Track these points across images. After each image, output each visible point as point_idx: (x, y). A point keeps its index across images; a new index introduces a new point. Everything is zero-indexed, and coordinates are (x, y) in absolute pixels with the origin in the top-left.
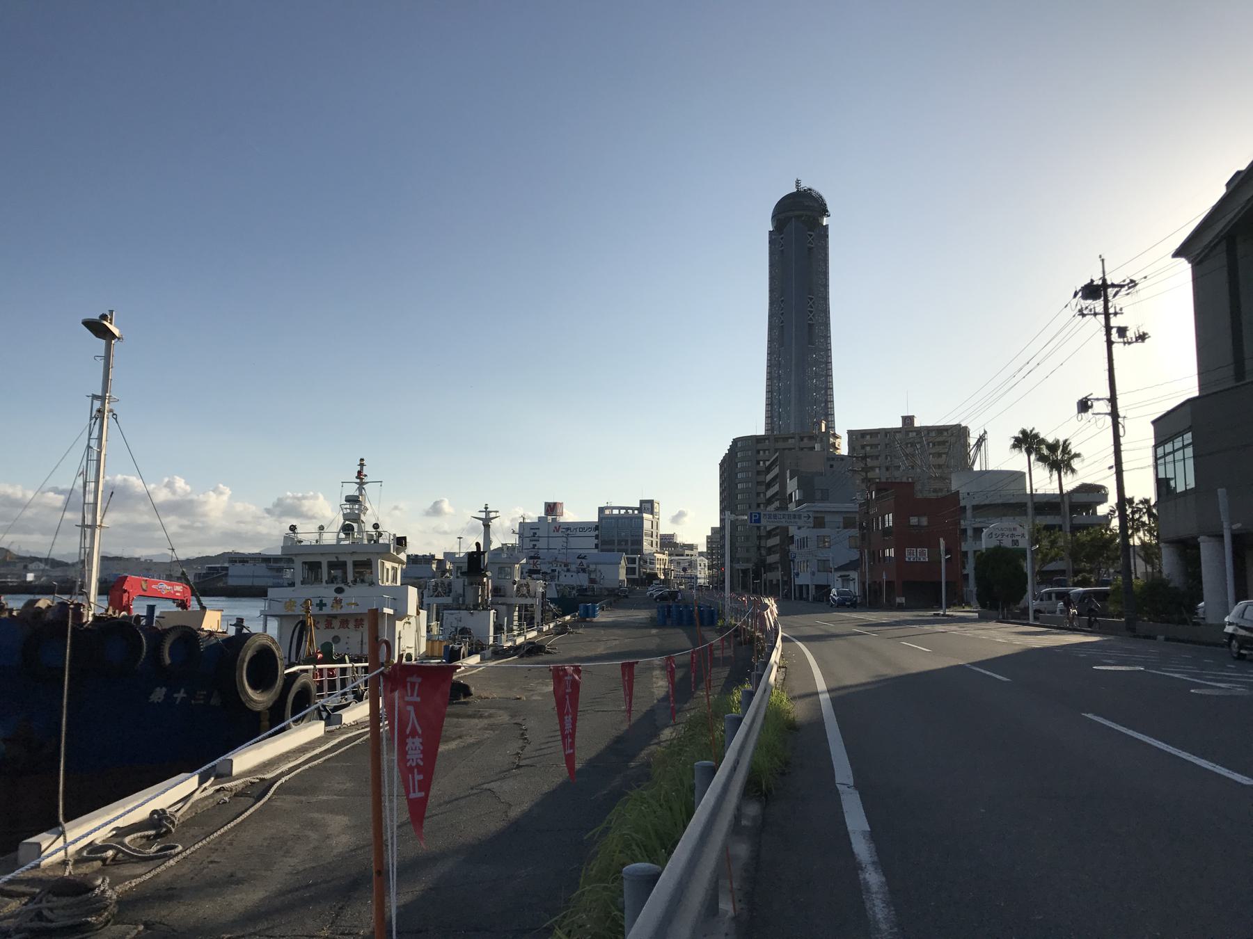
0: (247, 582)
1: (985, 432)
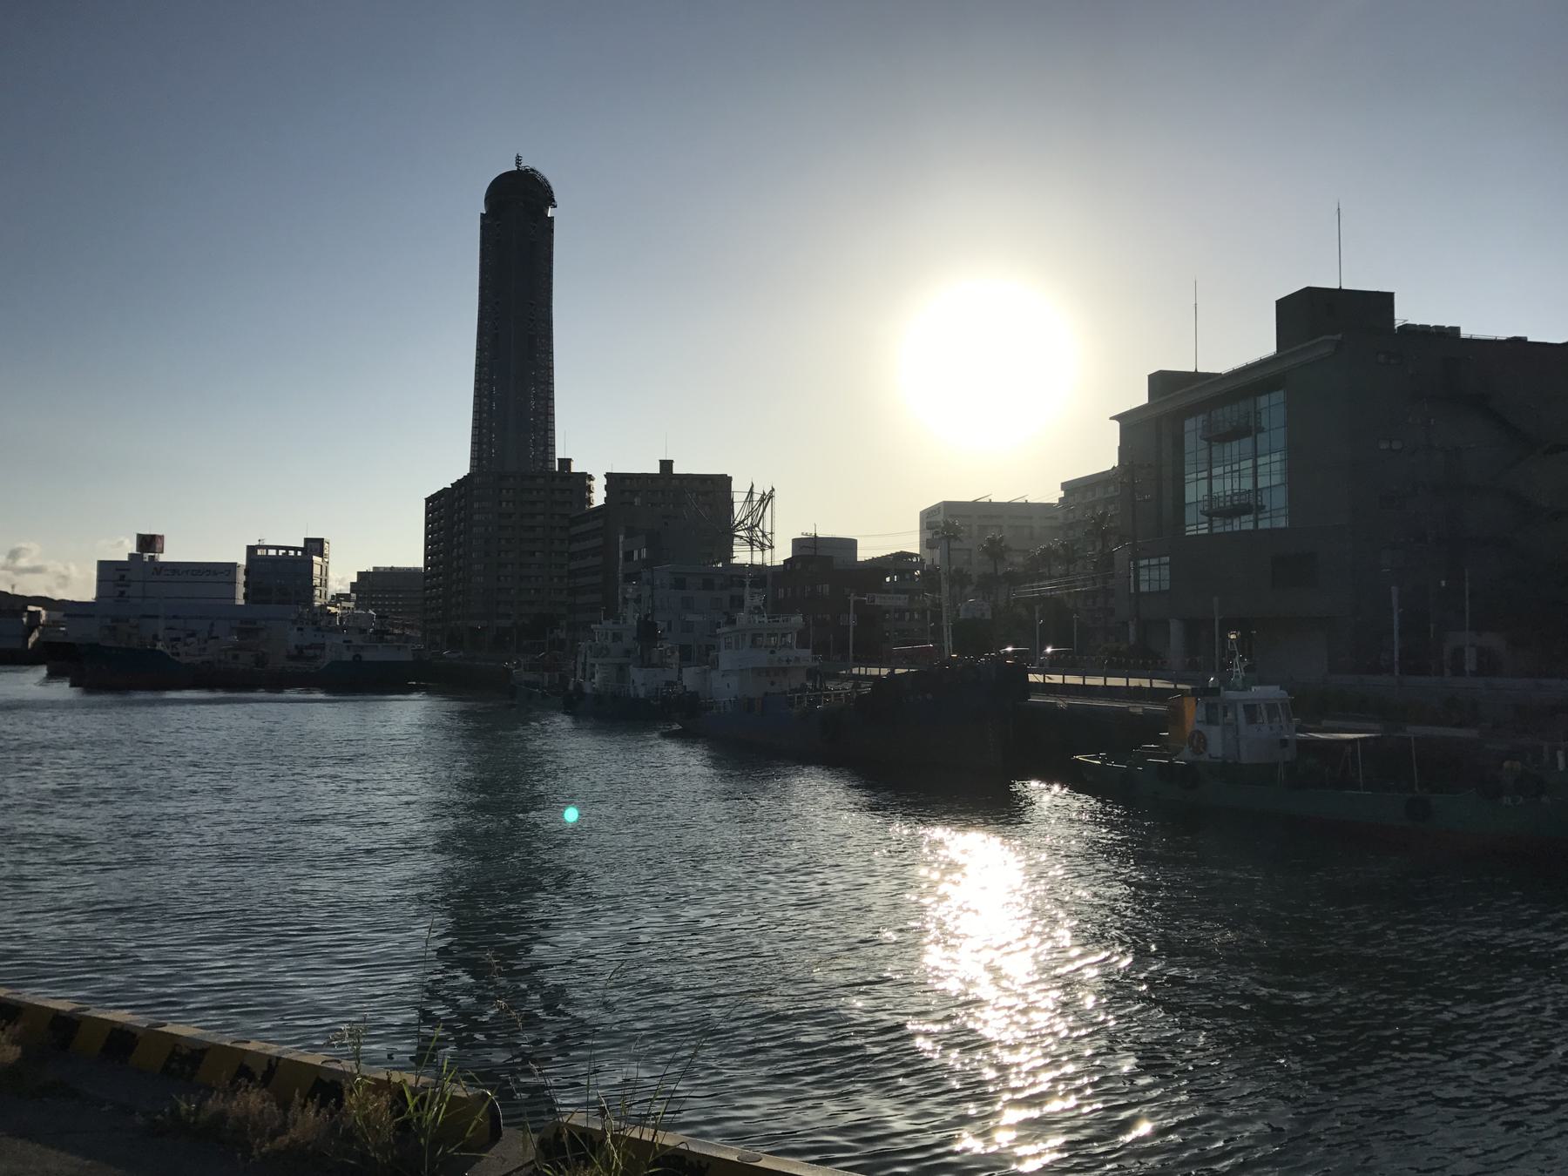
1: (773, 490)
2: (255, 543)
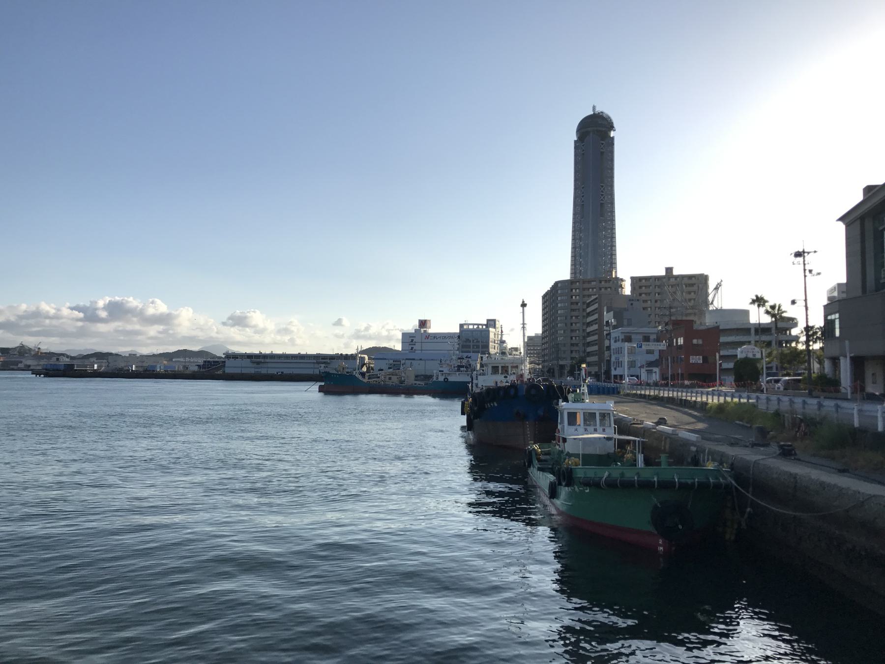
0: (238, 371)
1: (722, 281)
2: (463, 322)
